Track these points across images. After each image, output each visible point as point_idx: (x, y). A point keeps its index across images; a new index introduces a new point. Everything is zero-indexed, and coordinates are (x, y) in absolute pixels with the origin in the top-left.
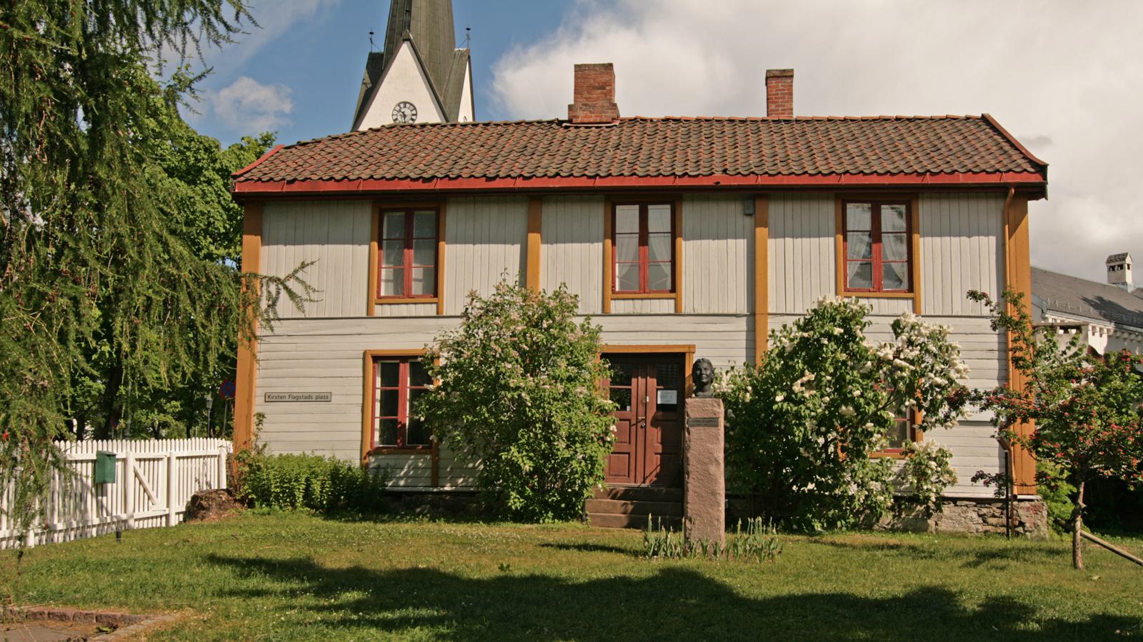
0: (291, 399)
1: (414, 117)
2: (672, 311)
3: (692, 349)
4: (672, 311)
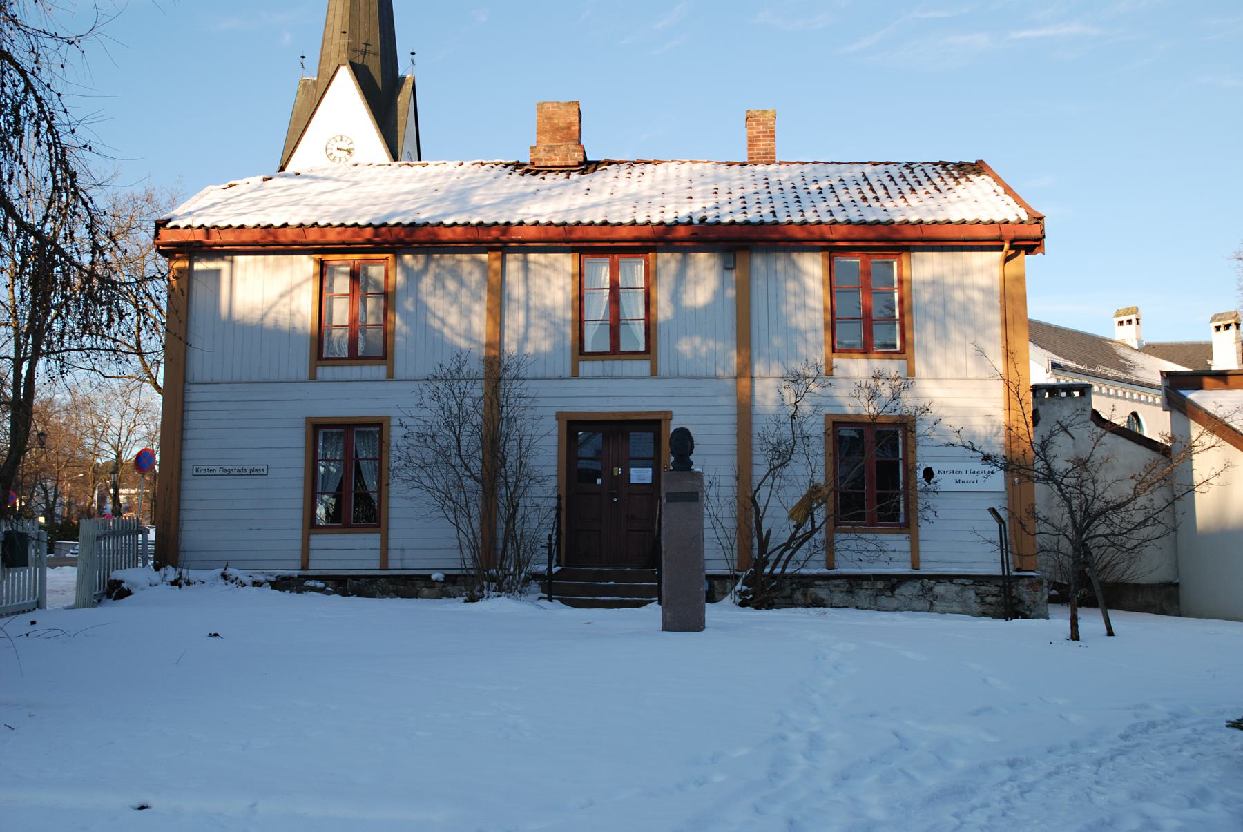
0: (221, 473)
1: (338, 139)
2: (607, 348)
3: (668, 415)
4: (607, 348)
